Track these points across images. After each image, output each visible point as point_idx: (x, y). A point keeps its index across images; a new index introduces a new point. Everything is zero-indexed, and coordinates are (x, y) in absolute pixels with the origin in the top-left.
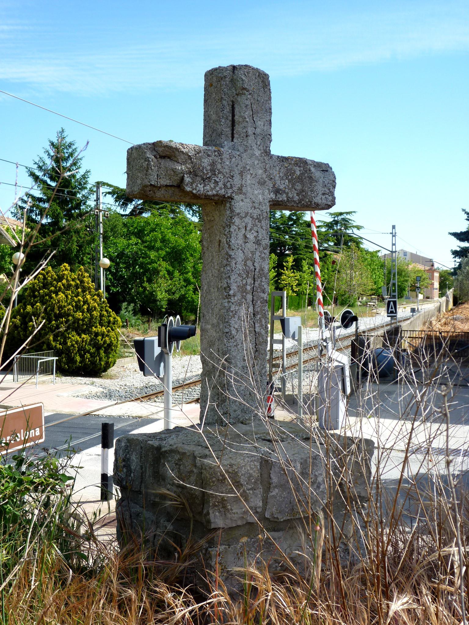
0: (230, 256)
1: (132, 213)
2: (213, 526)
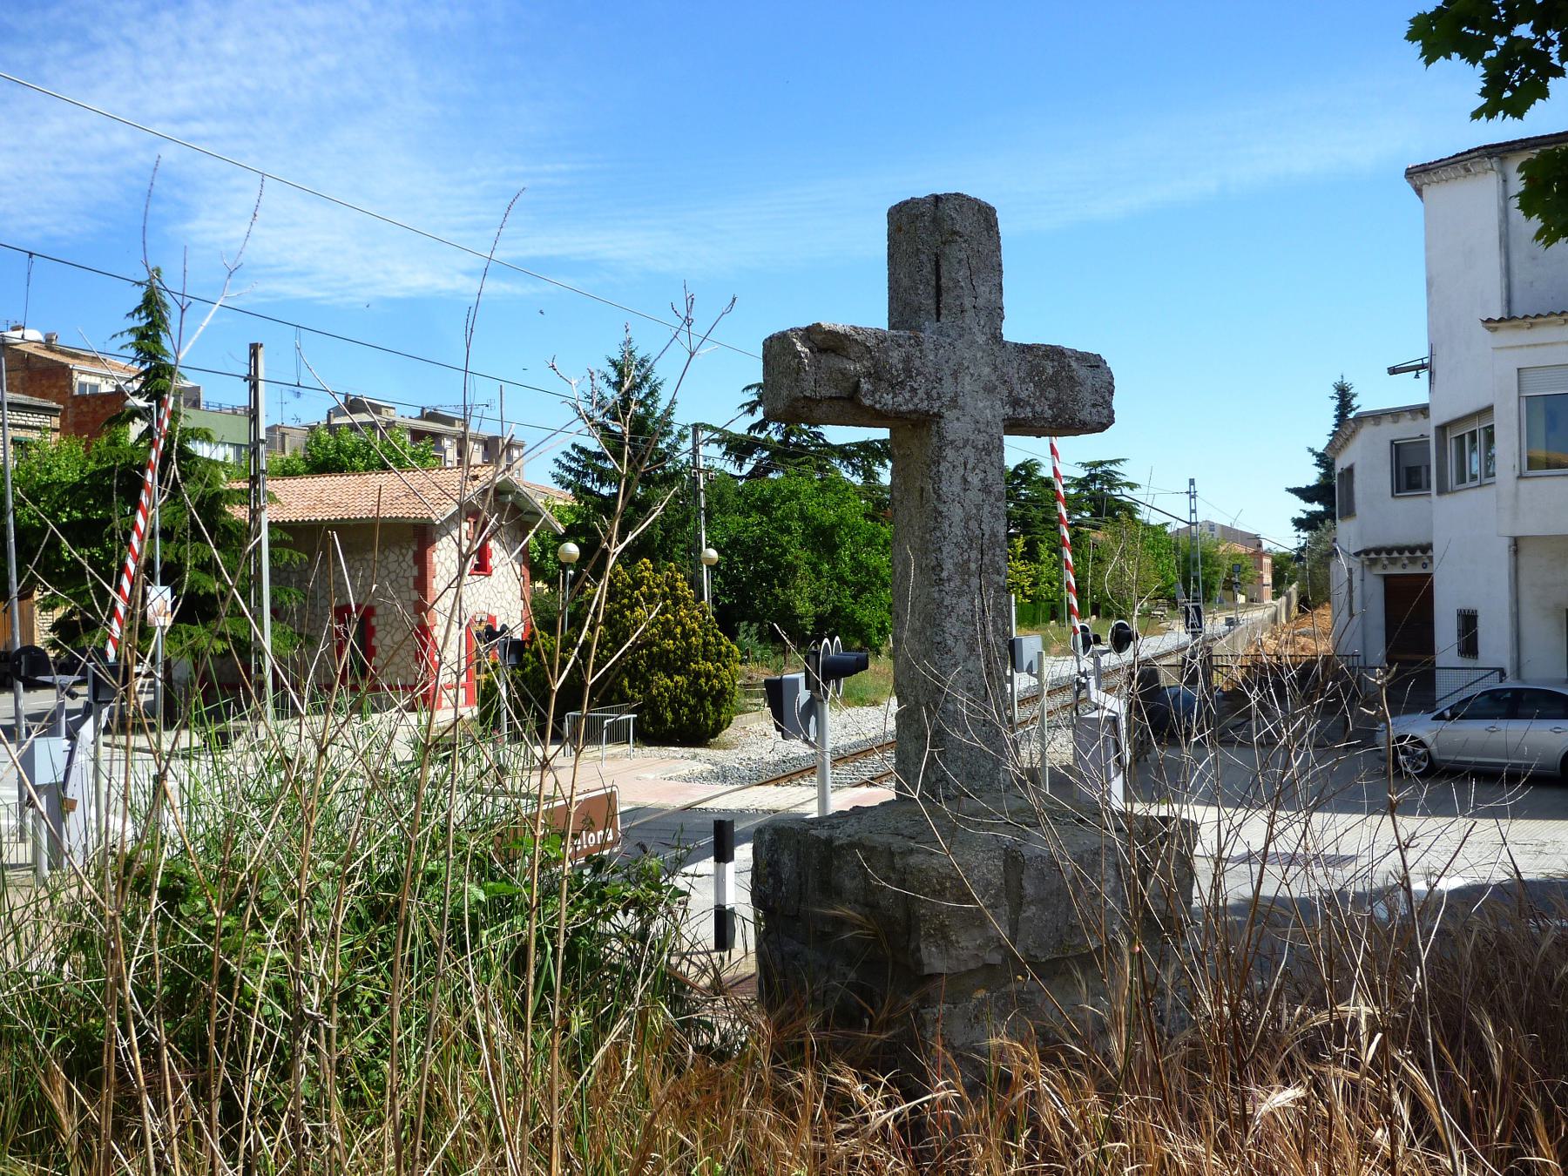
0: (940, 513)
1: (751, 475)
2: (927, 971)
